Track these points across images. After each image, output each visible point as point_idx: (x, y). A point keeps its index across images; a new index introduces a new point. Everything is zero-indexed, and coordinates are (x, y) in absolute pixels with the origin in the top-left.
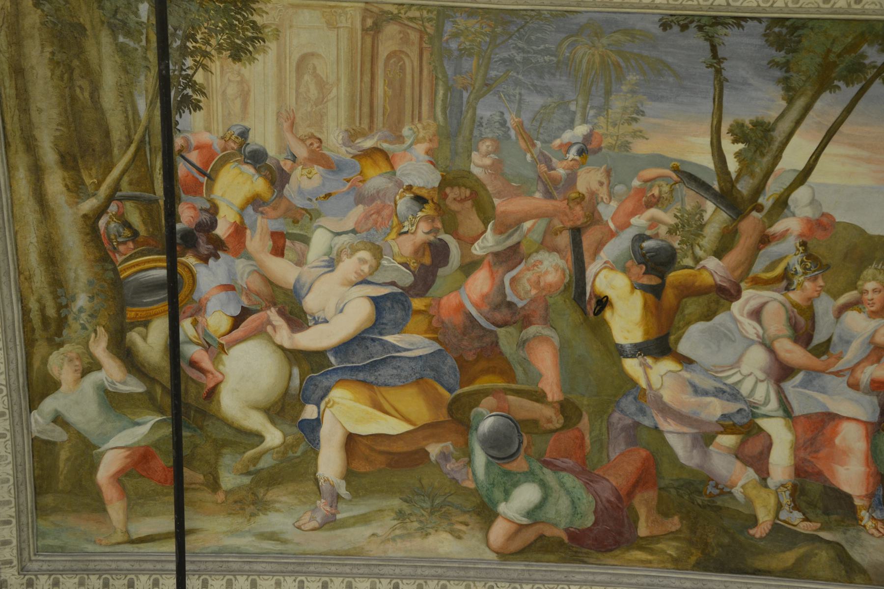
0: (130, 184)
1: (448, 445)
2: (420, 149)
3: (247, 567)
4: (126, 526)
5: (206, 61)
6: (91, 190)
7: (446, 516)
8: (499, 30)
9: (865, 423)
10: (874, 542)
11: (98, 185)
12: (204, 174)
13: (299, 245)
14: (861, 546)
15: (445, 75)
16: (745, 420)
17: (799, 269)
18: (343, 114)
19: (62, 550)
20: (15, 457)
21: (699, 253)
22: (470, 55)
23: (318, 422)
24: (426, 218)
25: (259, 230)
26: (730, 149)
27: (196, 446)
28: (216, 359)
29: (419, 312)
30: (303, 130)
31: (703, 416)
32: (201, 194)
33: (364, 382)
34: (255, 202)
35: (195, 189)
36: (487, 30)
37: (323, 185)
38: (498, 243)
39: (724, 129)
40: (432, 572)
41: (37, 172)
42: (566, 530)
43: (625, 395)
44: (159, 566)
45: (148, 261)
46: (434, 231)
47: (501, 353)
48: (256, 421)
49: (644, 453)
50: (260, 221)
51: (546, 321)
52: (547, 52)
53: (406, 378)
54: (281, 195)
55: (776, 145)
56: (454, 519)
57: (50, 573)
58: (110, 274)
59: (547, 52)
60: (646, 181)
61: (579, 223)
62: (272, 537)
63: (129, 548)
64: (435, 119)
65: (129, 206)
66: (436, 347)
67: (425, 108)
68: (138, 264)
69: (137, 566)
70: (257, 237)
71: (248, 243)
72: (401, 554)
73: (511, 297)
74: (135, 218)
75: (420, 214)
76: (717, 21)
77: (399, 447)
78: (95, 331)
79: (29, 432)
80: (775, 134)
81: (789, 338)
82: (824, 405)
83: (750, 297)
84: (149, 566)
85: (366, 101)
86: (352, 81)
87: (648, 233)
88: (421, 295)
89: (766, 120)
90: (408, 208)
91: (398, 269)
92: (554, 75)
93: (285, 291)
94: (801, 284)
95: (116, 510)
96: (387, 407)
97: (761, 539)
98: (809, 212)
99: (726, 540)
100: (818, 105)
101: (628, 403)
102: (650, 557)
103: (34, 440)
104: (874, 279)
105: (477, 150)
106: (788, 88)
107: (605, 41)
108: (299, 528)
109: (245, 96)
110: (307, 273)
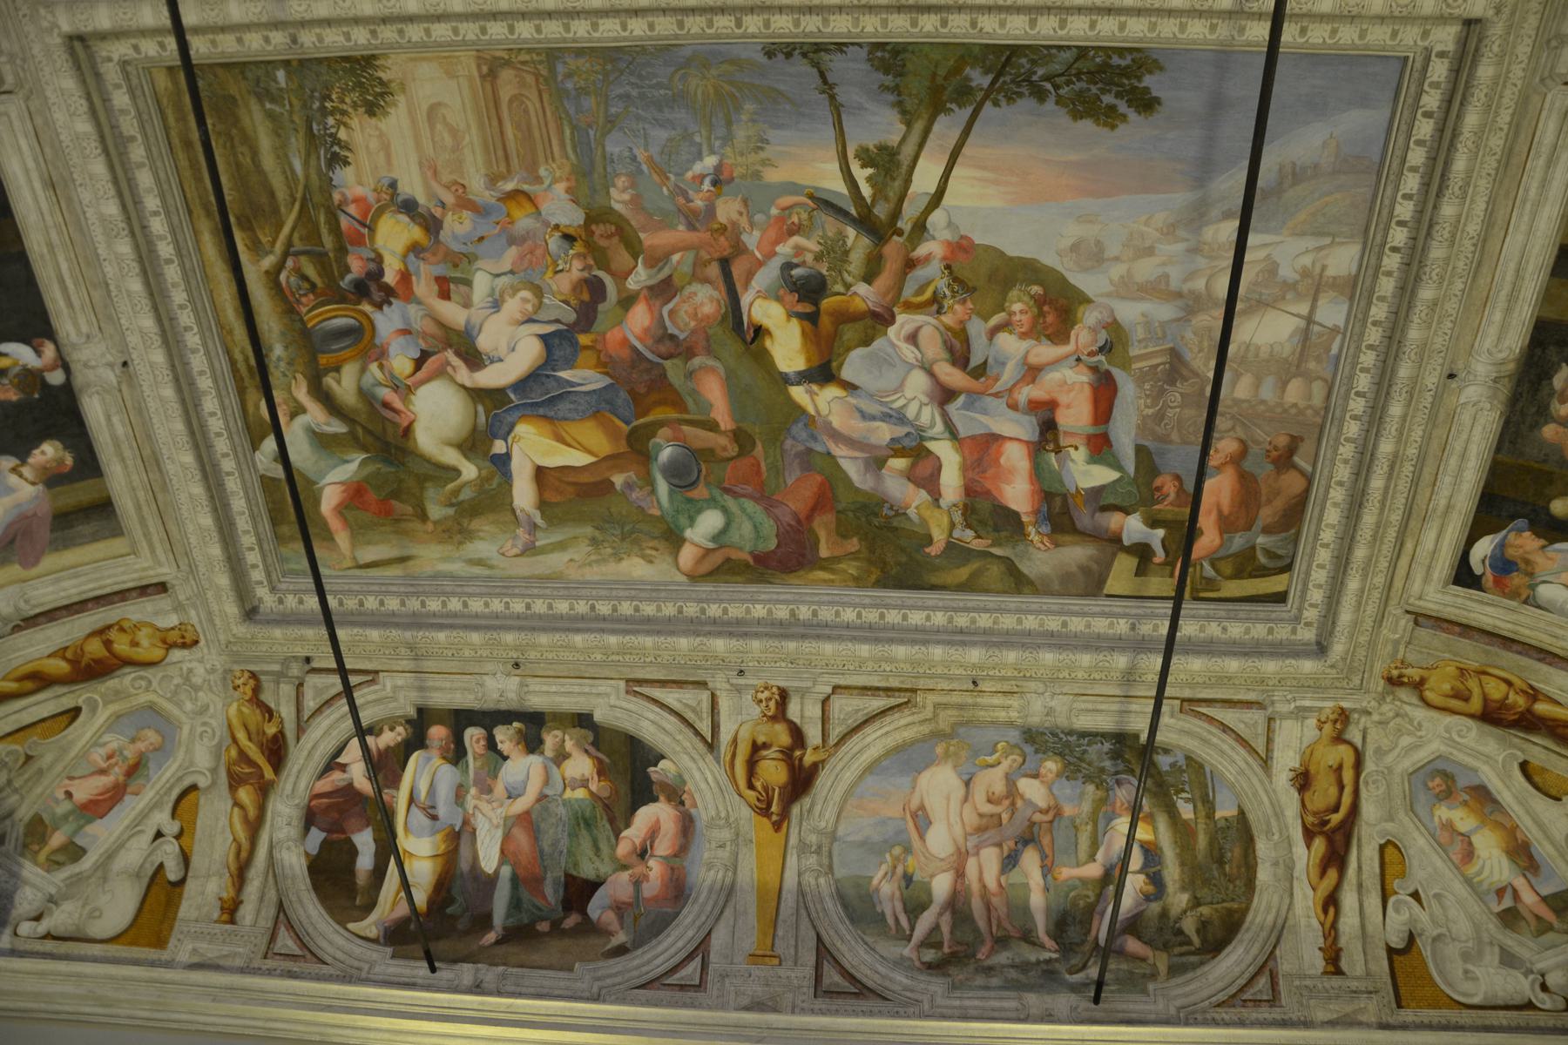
0: (301, 239)
2: (560, 188)
3: (459, 590)
4: (352, 552)
5: (346, 119)
6: (267, 247)
7: (636, 542)
8: (609, 67)
9: (1027, 443)
10: (1040, 555)
11: (273, 243)
12: (364, 225)
13: (463, 288)
14: (1029, 559)
15: (567, 114)
16: (914, 444)
17: (947, 293)
18: (480, 159)
20: (246, 493)
21: (849, 279)
22: (588, 94)
23: (507, 457)
24: (578, 255)
25: (423, 276)
26: (861, 174)
27: (401, 481)
29: (586, 348)
30: (446, 177)
31: (873, 440)
32: (365, 244)
33: (545, 417)
34: (415, 249)
35: (359, 241)
36: (598, 68)
37: (475, 229)
38: (650, 277)
39: (851, 154)
40: (627, 593)
42: (751, 553)
43: (796, 421)
44: (383, 588)
45: (329, 311)
46: (587, 268)
47: (670, 385)
48: (451, 457)
49: (819, 478)
50: (423, 267)
51: (709, 351)
52: (659, 86)
53: (583, 412)
54: (437, 241)
55: (904, 169)
56: (644, 545)
57: (295, 592)
58: (298, 325)
59: (659, 86)
60: (784, 209)
61: (725, 253)
62: (480, 562)
63: (358, 572)
64: (568, 158)
65: (303, 260)
66: (608, 381)
67: (556, 149)
68: (321, 314)
69: (365, 588)
70: (423, 282)
71: (415, 288)
72: (596, 578)
73: (672, 330)
74: (310, 271)
75: (571, 252)
76: (819, 48)
77: (585, 478)
78: (295, 378)
79: (256, 470)
80: (901, 157)
81: (947, 361)
82: (987, 426)
83: (904, 322)
84: (376, 588)
85: (499, 145)
86: (481, 126)
87: (795, 261)
88: (586, 330)
89: (890, 144)
90: (559, 247)
91: (560, 307)
92: (672, 108)
94: (951, 307)
95: (342, 539)
96: (569, 439)
97: (937, 556)
98: (947, 235)
99: (904, 559)
100: (936, 128)
101: (798, 430)
102: (832, 577)
103: (262, 477)
105: (614, 186)
106: (904, 112)
107: (714, 72)
108: (503, 554)
109: (386, 148)
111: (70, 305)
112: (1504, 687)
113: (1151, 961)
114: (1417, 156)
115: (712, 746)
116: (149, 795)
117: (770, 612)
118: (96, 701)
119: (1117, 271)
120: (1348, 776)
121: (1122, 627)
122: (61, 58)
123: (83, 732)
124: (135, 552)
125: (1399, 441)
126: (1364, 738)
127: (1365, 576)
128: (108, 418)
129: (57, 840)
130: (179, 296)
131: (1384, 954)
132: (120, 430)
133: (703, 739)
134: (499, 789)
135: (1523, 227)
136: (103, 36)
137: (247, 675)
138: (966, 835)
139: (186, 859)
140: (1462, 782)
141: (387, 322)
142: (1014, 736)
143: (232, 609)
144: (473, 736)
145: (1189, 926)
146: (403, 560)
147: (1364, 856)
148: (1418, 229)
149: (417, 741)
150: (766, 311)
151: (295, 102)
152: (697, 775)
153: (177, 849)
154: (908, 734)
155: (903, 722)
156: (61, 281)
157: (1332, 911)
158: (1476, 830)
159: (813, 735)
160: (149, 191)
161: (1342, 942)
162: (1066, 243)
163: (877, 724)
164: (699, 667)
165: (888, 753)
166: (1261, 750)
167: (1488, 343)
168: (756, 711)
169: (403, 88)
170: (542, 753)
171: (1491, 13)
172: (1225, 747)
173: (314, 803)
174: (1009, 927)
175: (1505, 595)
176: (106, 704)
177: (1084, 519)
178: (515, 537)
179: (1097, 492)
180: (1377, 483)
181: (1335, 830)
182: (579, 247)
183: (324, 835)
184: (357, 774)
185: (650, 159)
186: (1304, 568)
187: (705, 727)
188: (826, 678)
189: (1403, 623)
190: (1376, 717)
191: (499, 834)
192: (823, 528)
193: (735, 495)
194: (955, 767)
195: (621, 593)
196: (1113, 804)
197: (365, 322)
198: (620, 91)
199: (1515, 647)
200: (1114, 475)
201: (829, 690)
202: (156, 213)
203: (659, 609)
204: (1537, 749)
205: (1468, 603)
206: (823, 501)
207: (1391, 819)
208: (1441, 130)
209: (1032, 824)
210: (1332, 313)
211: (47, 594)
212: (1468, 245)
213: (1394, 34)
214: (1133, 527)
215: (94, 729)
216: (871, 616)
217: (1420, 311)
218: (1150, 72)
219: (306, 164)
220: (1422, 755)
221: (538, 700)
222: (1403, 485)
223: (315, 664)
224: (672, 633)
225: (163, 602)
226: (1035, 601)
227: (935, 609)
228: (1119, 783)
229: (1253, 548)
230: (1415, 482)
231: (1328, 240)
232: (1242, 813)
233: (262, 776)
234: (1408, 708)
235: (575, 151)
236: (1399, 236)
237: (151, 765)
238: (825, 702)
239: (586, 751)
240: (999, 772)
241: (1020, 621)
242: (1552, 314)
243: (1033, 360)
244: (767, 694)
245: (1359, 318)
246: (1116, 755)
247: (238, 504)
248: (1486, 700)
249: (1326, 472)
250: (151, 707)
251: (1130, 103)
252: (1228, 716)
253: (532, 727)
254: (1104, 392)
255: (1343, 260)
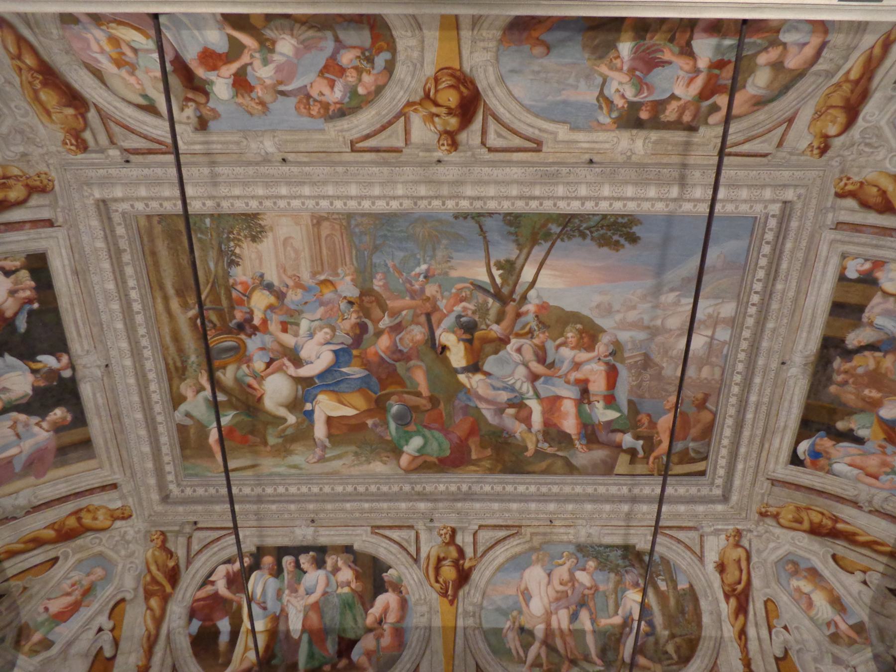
0: (210, 302)
1: (377, 420)
5: (240, 243)
10: (582, 455)
12: (244, 295)
13: (295, 327)
18: (308, 264)
19: (196, 475)
21: (488, 322)
22: (366, 234)
23: (311, 412)
26: (496, 273)
28: (260, 384)
29: (356, 356)
30: (290, 273)
31: (499, 400)
33: (333, 391)
34: (271, 307)
35: (241, 303)
39: (492, 263)
41: (166, 299)
42: (437, 458)
46: (359, 317)
48: (282, 412)
49: (471, 419)
50: (274, 316)
51: (419, 358)
52: (402, 231)
57: (191, 486)
59: (402, 231)
62: (295, 467)
66: (366, 373)
67: (348, 259)
70: (274, 324)
72: (358, 473)
73: (400, 347)
76: (480, 215)
77: (353, 422)
79: (174, 419)
83: (515, 342)
86: (310, 249)
93: (290, 350)
94: (538, 336)
98: (537, 301)
99: (514, 459)
101: (461, 395)
104: (571, 331)
106: (519, 245)
107: (429, 225)
109: (260, 258)
110: (300, 340)
111: (79, 335)
112: (820, 516)
113: (653, 669)
114: (763, 262)
115: (416, 560)
116: (95, 606)
117: (447, 488)
118: (68, 553)
119: (618, 317)
120: (744, 564)
121: (625, 490)
122: (92, 211)
123: (59, 571)
124: (101, 467)
125: (759, 395)
126: (750, 544)
127: (745, 462)
128: (94, 394)
129: (36, 637)
130: (142, 331)
131: (773, 661)
132: (100, 401)
133: (412, 556)
134: (301, 590)
135: (815, 293)
136: (116, 200)
137: (159, 533)
138: (550, 603)
139: (116, 643)
140: (803, 566)
141: (253, 344)
142: (572, 548)
143: (155, 496)
144: (287, 561)
145: (670, 648)
146: (253, 466)
147: (756, 607)
148: (764, 295)
149: (256, 565)
150: (447, 338)
151: (214, 234)
152: (409, 576)
153: (111, 638)
154: (518, 549)
155: (515, 543)
156: (76, 322)
157: (743, 637)
158: (812, 591)
159: (469, 551)
160: (131, 277)
161: (751, 655)
162: (594, 304)
163: (502, 544)
164: (410, 518)
165: (508, 560)
166: (698, 551)
167: (800, 347)
168: (439, 540)
169: (271, 229)
170: (325, 568)
171: (795, 198)
172: (679, 551)
173: (195, 604)
174: (576, 653)
175: (817, 469)
176: (74, 554)
177: (603, 436)
178: (314, 453)
179: (609, 423)
180: (749, 416)
181: (740, 594)
182: (355, 307)
183: (200, 623)
184: (221, 587)
185: (394, 266)
186: (714, 458)
187: (413, 550)
188: (475, 521)
189: (765, 484)
190: (755, 533)
191: (301, 616)
192: (473, 444)
193: (430, 428)
194: (542, 566)
195: (370, 481)
196: (625, 584)
197: (242, 345)
198: (382, 233)
199: (824, 495)
200: (617, 415)
201: (476, 527)
202: (133, 288)
203: (390, 488)
204: (840, 547)
205: (799, 474)
206: (473, 430)
207: (768, 586)
208: (774, 250)
209: (584, 595)
210: (723, 334)
211: (47, 492)
212: (789, 303)
213: (751, 207)
214: (627, 440)
215: (67, 567)
216: (498, 488)
217: (767, 333)
218: (636, 225)
219: (216, 265)
220: (780, 552)
221: (323, 540)
222: (762, 416)
223: (199, 526)
224: (397, 500)
225: (114, 494)
226: (577, 478)
227: (530, 484)
228: (627, 572)
229: (687, 449)
230: (768, 415)
231: (720, 301)
232: (691, 586)
233: (165, 591)
234: (771, 528)
235: (357, 259)
236: (755, 298)
237: (98, 588)
238: (475, 534)
239: (350, 566)
240: (565, 568)
241: (573, 489)
242: (831, 334)
243: (577, 360)
244: (445, 531)
245: (736, 337)
246: (624, 557)
247: (164, 439)
248: (811, 523)
249: (723, 411)
250: (101, 555)
251: (626, 239)
252: (681, 535)
253: (320, 554)
254: (612, 375)
255: (728, 309)
